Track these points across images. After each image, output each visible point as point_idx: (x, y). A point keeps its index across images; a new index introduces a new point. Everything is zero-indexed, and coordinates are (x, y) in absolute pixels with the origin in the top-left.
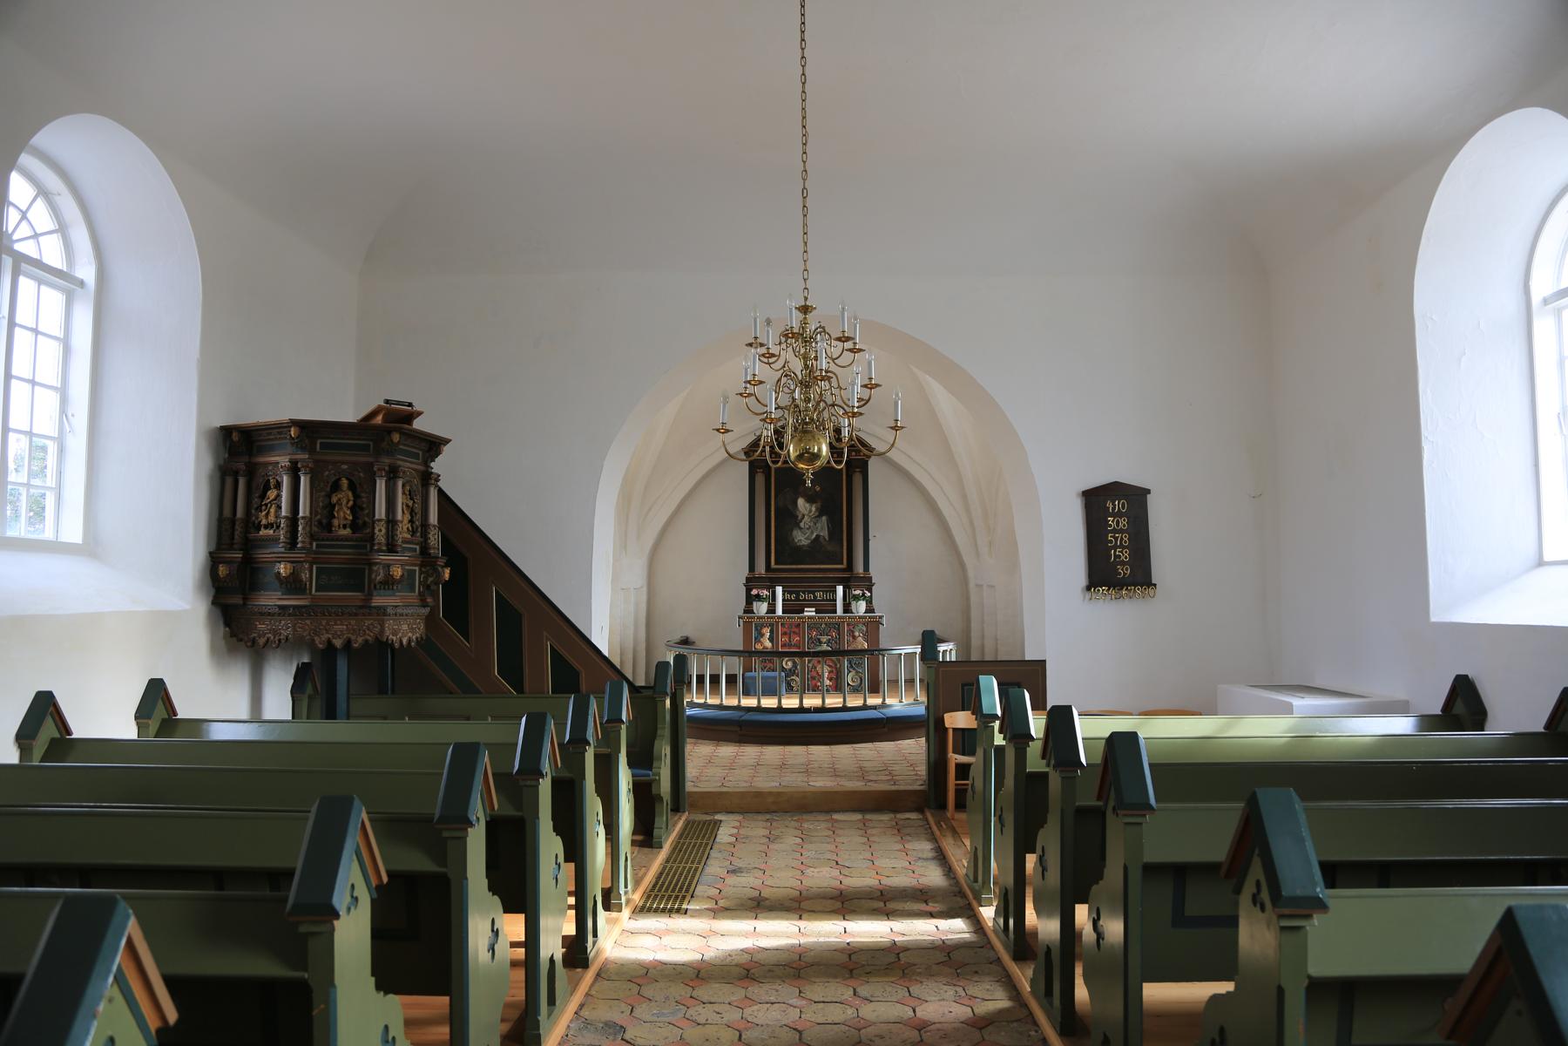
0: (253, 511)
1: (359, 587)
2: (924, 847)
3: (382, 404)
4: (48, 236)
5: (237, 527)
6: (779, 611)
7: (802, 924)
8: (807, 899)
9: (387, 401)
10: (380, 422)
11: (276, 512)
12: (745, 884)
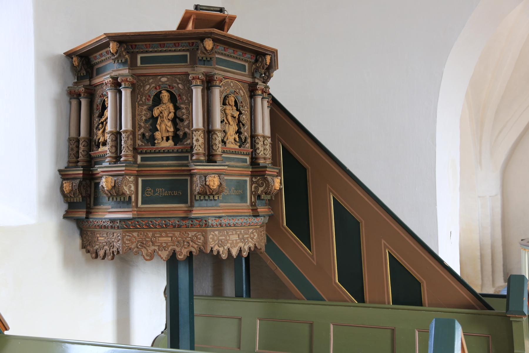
0: (95, 130)
1: (183, 200)
5: (81, 146)
9: (197, 7)
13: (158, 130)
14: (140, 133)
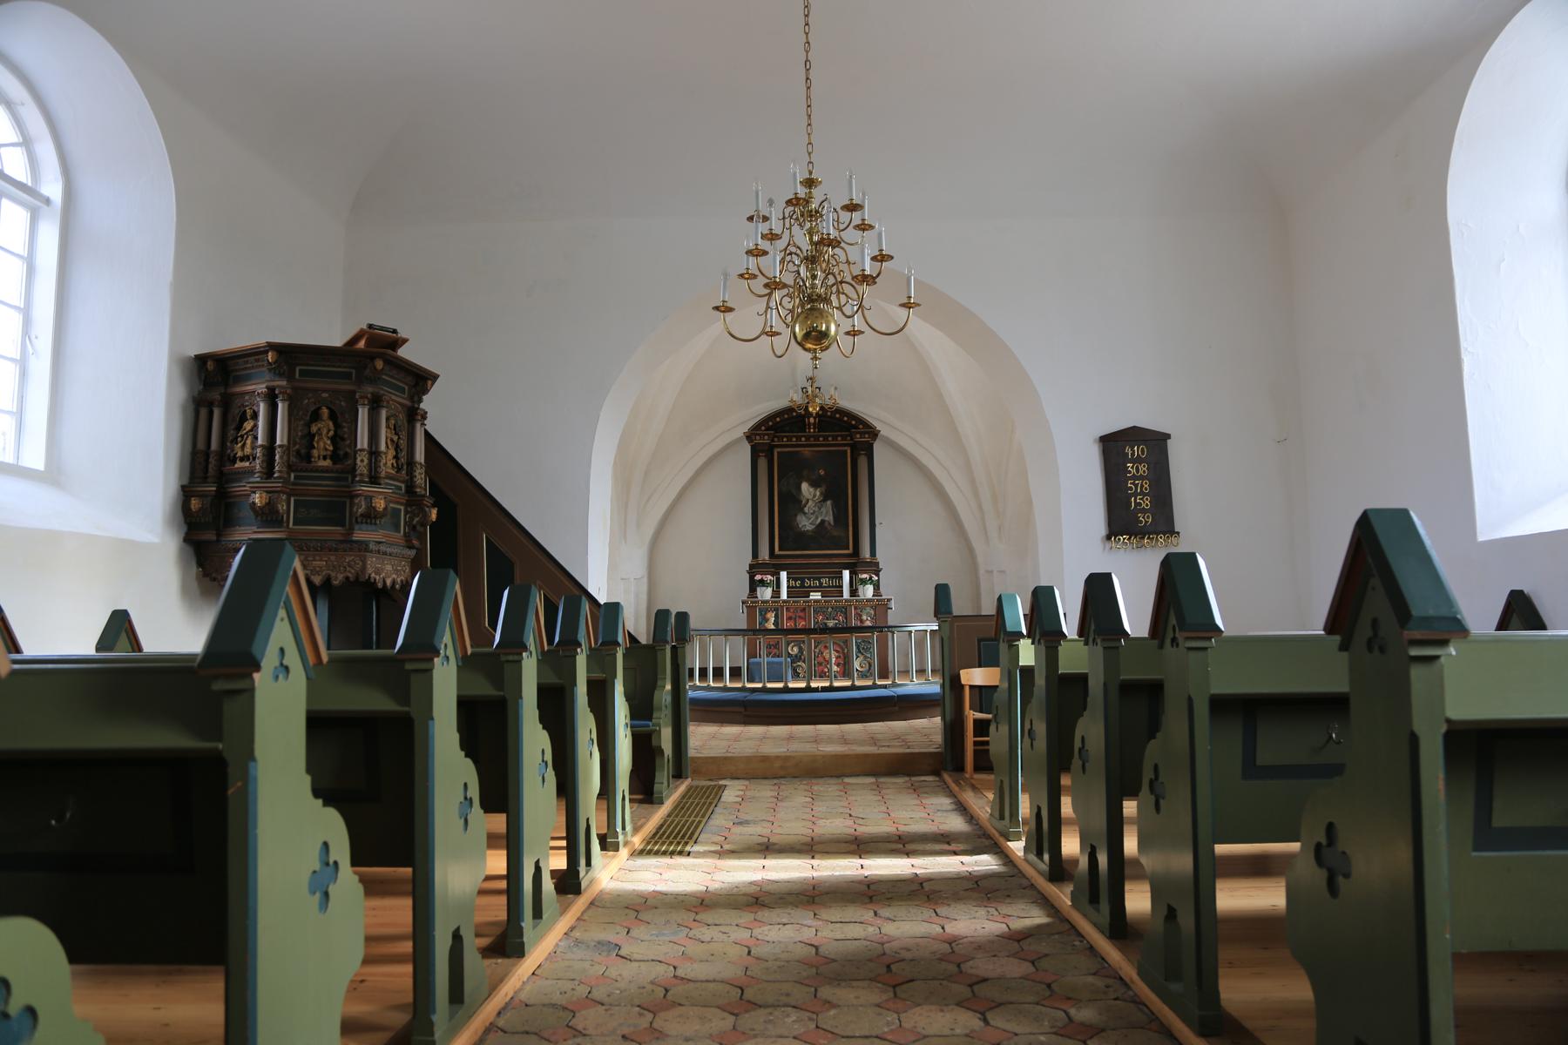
0: (229, 444)
2: (945, 802)
3: (365, 327)
4: (11, 148)
5: (210, 460)
6: (784, 596)
7: (815, 862)
8: (821, 843)
9: (370, 326)
10: (363, 347)
11: (252, 443)
12: (755, 832)
13: (314, 448)
14: (294, 449)
